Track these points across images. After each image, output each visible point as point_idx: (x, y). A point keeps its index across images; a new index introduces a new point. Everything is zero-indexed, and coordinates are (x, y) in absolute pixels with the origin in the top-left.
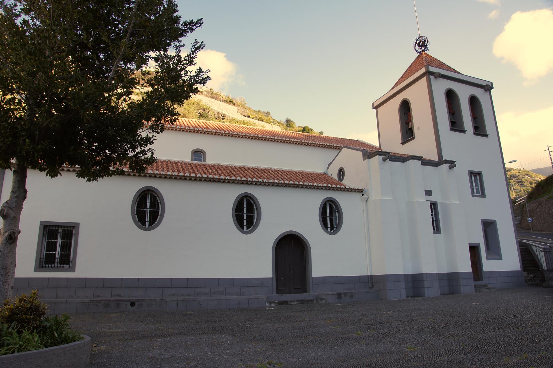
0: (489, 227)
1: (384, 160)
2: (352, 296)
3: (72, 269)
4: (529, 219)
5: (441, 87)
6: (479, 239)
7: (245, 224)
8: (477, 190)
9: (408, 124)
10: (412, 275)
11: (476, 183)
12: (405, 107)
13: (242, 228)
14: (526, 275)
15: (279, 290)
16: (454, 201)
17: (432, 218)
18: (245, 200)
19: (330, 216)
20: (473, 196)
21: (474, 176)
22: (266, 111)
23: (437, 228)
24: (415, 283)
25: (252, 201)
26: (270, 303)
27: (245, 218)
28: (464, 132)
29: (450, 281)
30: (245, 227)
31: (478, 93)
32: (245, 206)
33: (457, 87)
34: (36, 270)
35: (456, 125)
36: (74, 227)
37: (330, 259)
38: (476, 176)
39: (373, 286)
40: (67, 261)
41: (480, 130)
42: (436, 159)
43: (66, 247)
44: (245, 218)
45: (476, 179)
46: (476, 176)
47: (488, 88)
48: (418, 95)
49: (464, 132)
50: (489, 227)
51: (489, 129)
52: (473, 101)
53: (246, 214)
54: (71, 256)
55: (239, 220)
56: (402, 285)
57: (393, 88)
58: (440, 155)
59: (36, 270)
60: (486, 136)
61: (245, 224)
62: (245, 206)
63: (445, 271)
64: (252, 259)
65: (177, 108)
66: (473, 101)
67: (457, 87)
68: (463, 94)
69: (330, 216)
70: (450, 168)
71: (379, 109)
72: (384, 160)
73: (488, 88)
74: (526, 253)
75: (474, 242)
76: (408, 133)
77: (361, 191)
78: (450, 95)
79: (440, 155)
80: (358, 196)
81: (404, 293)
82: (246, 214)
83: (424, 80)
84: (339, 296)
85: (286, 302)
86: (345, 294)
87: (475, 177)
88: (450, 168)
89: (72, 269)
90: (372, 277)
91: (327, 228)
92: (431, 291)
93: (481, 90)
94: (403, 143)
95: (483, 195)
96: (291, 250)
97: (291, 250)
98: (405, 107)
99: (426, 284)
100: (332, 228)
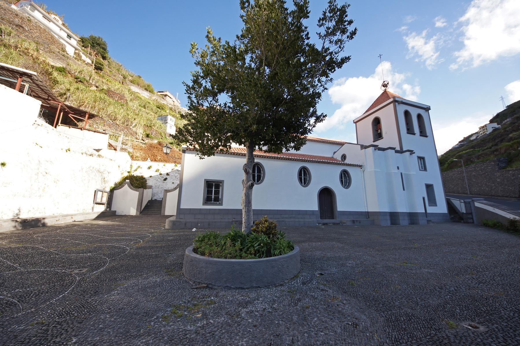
0: (429, 188)
1: (375, 150)
2: (360, 222)
3: (221, 204)
5: (401, 109)
8: (422, 167)
9: (377, 131)
11: (421, 163)
12: (377, 122)
15: (322, 218)
16: (412, 173)
19: (345, 179)
20: (420, 170)
24: (394, 217)
26: (319, 224)
28: (414, 134)
31: (422, 112)
34: (203, 205)
35: (410, 131)
36: (221, 182)
37: (345, 202)
38: (421, 159)
39: (369, 217)
40: (218, 200)
41: (423, 133)
42: (398, 148)
43: (217, 193)
45: (421, 161)
46: (421, 159)
47: (427, 109)
49: (414, 134)
50: (429, 188)
51: (428, 133)
52: (419, 116)
53: (304, 177)
54: (220, 197)
55: (300, 179)
56: (388, 218)
57: (366, 112)
58: (401, 147)
59: (203, 205)
60: (427, 137)
64: (308, 201)
65: (336, 69)
66: (419, 116)
67: (409, 109)
68: (414, 113)
69: (345, 179)
70: (411, 154)
72: (375, 150)
73: (427, 109)
76: (378, 135)
77: (360, 166)
78: (407, 114)
79: (401, 147)
80: (359, 169)
81: (389, 222)
82: (304, 177)
83: (392, 105)
84: (353, 222)
85: (327, 224)
86: (357, 221)
87: (420, 160)
88: (411, 154)
89: (221, 204)
91: (302, 183)
92: (404, 222)
93: (423, 111)
95: (425, 169)
96: (326, 195)
97: (326, 195)
98: (377, 122)
99: (401, 218)
100: (305, 183)
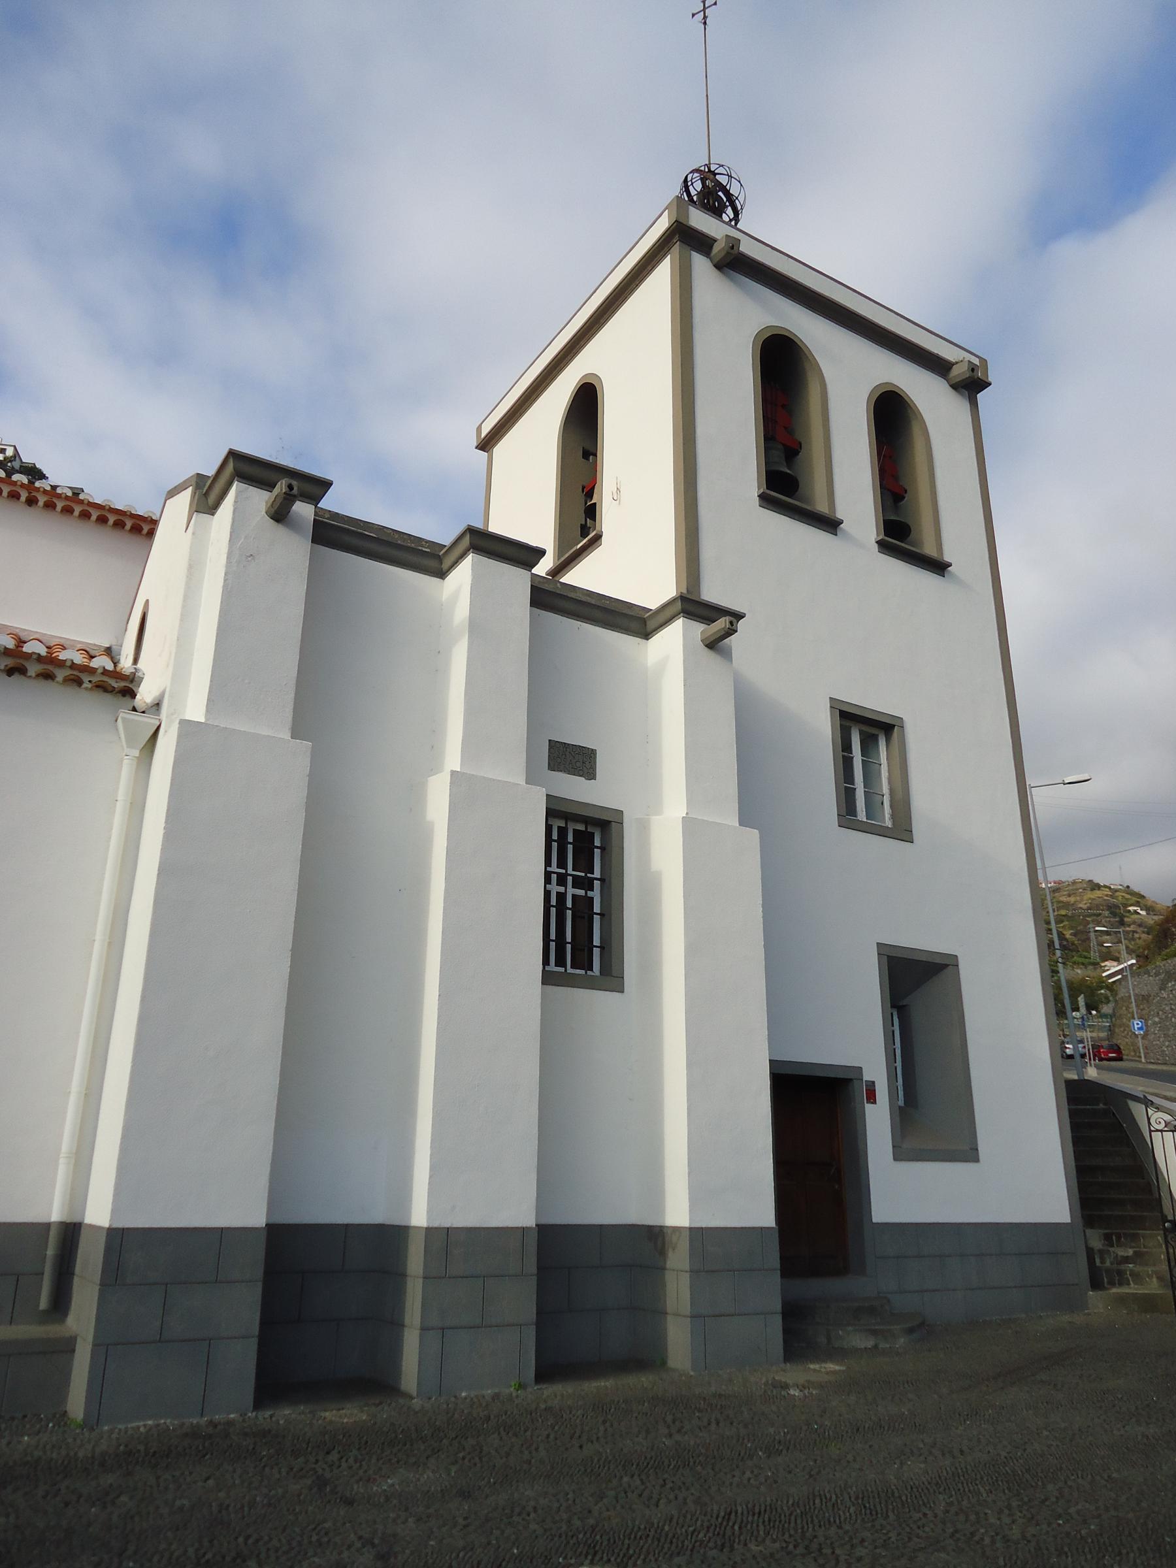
0: (915, 984)
4: (1137, 1024)
5: (736, 319)
6: (856, 1040)
14: (1097, 1243)
17: (547, 894)
22: (280, 531)
29: (580, 1279)
31: (927, 394)
35: (787, 483)
48: (634, 363)
50: (915, 984)
51: (956, 536)
52: (891, 415)
66: (891, 415)
71: (499, 450)
74: (1098, 1130)
75: (823, 1050)
78: (781, 368)
80: (88, 706)
87: (869, 743)
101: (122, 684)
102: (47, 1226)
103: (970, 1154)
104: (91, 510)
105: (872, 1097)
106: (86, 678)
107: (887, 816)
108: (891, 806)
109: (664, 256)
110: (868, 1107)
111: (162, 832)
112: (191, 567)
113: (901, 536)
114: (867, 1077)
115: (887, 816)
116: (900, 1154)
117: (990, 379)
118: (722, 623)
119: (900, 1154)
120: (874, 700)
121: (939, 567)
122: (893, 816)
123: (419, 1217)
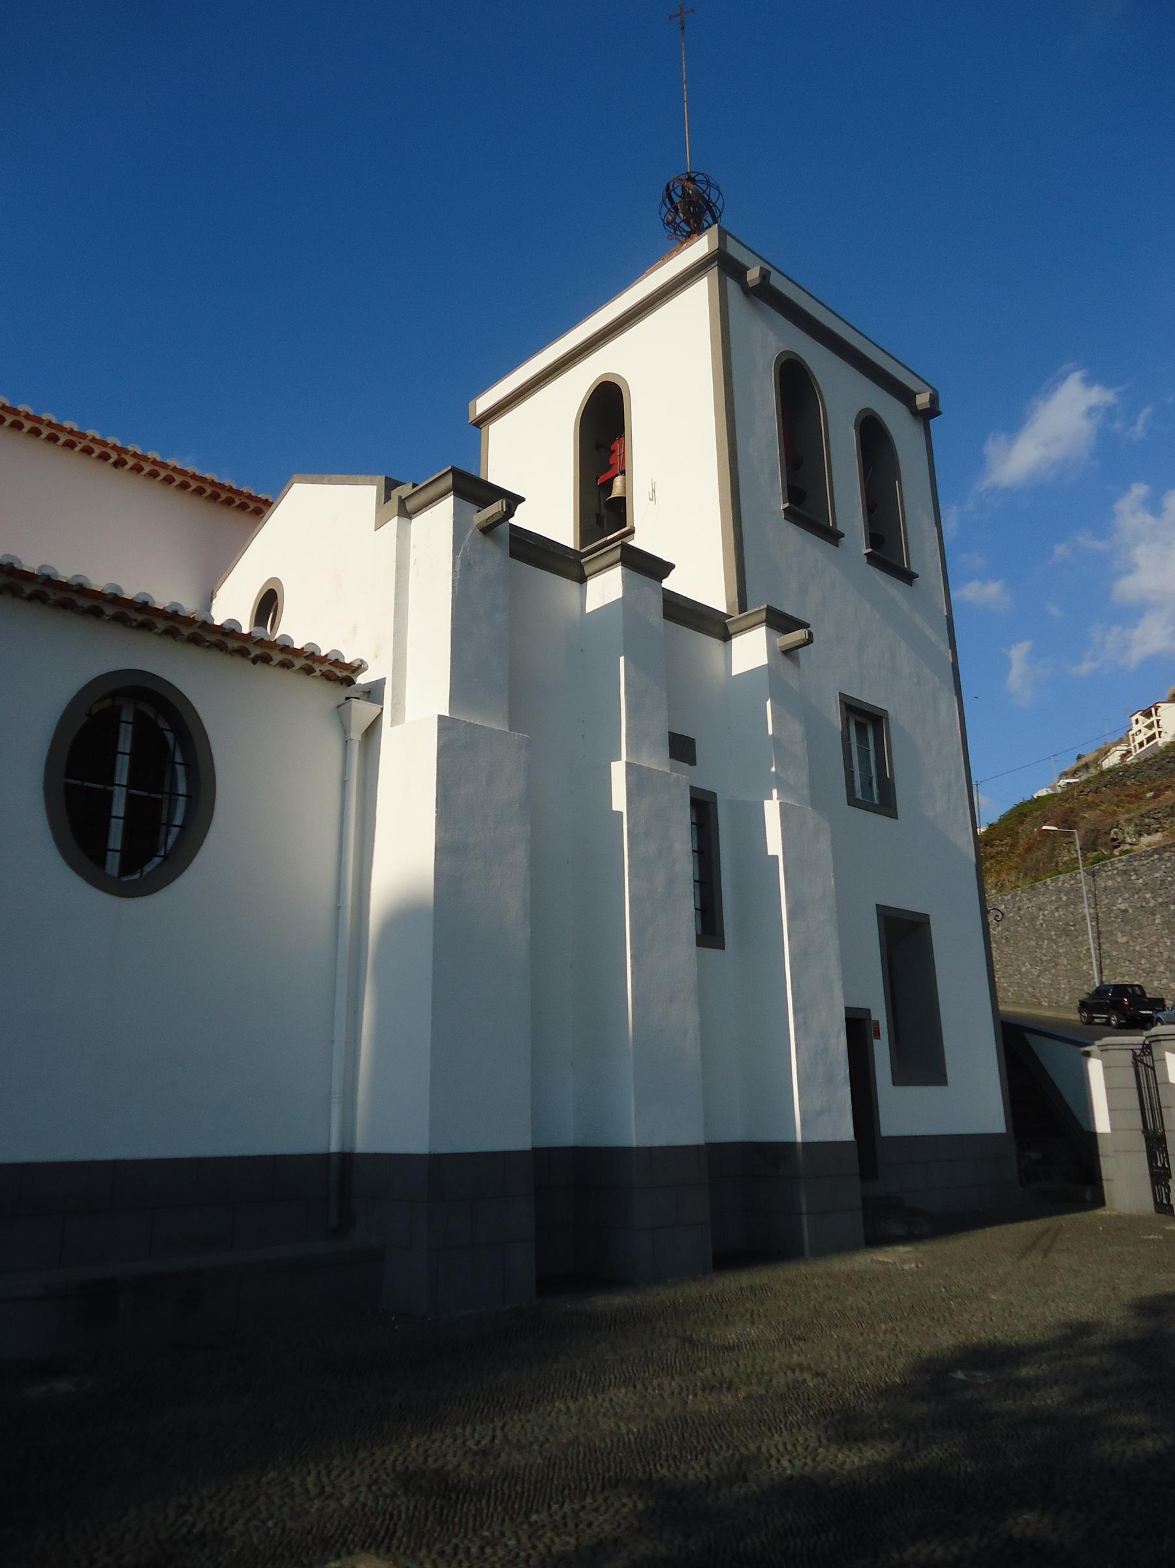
7: (115, 839)
8: (867, 784)
10: (575, 1149)
13: (100, 860)
18: (127, 715)
21: (858, 725)
22: (489, 544)
23: (710, 930)
25: (162, 724)
27: (119, 807)
30: (113, 862)
32: (125, 744)
33: (822, 363)
35: (806, 505)
44: (119, 807)
51: (920, 551)
52: (871, 432)
61: (115, 839)
62: (125, 744)
63: (511, 1134)
66: (871, 432)
67: (822, 363)
68: (843, 396)
87: (861, 729)
90: (347, 1160)
94: (522, 500)
101: (345, 673)
102: (328, 1156)
103: (939, 1078)
104: (176, 476)
105: (877, 1035)
106: (318, 668)
107: (875, 796)
108: (878, 787)
109: (701, 277)
110: (875, 1042)
111: (434, 815)
112: (398, 568)
113: (887, 553)
114: (874, 1017)
115: (875, 796)
116: (896, 1082)
117: (941, 409)
118: (799, 635)
119: (896, 1082)
120: (871, 697)
121: (908, 577)
122: (880, 796)
123: (799, 1139)
